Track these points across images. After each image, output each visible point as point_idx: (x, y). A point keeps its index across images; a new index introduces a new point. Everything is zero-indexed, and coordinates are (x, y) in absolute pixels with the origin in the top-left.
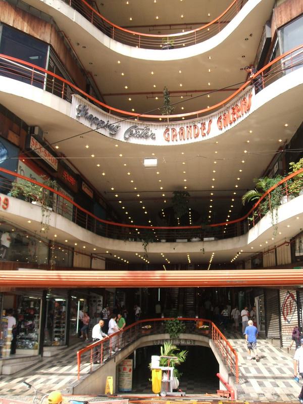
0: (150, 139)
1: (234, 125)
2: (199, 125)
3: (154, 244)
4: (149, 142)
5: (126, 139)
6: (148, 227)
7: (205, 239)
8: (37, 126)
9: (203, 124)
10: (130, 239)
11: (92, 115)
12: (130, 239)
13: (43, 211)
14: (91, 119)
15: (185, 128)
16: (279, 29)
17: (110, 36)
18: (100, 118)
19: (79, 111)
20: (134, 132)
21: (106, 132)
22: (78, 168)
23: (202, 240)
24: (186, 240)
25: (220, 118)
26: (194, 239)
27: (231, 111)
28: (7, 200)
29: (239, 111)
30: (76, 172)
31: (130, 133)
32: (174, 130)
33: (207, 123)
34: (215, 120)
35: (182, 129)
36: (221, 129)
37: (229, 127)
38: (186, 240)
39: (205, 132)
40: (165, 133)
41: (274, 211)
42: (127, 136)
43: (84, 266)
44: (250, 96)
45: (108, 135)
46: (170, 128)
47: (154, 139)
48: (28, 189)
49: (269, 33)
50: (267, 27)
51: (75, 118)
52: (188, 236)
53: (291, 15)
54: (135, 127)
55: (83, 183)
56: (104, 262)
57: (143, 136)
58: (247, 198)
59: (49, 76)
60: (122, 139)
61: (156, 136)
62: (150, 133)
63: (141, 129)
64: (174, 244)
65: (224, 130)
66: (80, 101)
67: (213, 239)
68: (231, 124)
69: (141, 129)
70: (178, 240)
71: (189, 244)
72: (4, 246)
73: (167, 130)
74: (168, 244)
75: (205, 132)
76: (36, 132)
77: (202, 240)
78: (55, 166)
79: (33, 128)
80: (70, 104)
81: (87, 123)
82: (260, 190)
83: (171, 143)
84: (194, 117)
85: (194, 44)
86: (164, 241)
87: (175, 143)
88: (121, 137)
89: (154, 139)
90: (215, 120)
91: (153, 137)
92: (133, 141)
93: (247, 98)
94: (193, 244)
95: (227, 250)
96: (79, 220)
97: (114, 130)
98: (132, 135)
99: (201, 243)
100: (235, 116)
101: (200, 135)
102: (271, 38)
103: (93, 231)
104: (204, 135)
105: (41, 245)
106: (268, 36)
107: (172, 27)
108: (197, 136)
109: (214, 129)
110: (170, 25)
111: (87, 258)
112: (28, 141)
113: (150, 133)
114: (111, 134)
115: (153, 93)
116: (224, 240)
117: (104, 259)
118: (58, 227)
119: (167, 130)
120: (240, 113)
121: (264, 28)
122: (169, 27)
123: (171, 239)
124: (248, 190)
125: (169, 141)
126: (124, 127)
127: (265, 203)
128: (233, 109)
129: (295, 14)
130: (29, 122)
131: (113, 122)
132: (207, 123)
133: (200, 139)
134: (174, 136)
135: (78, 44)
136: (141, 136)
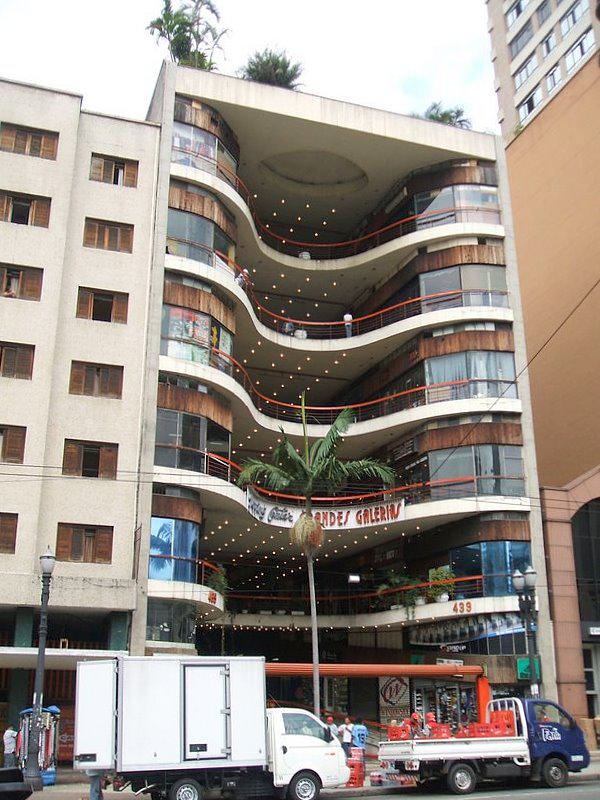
1: (375, 524)
2: (336, 515)
5: (269, 521)
24: (303, 613)
26: (280, 612)
31: (273, 516)
33: (344, 515)
37: (370, 524)
39: (342, 521)
41: (410, 609)
43: (562, 666)
47: (291, 521)
67: (303, 613)
68: (373, 521)
70: (262, 612)
71: (274, 616)
74: (253, 616)
75: (342, 521)
83: (363, 526)
84: (584, 481)
86: (246, 612)
92: (275, 523)
94: (279, 618)
95: (57, 607)
105: (44, 617)
108: (332, 524)
111: (563, 686)
123: (254, 611)
126: (269, 508)
129: (555, 580)
135: (374, 269)
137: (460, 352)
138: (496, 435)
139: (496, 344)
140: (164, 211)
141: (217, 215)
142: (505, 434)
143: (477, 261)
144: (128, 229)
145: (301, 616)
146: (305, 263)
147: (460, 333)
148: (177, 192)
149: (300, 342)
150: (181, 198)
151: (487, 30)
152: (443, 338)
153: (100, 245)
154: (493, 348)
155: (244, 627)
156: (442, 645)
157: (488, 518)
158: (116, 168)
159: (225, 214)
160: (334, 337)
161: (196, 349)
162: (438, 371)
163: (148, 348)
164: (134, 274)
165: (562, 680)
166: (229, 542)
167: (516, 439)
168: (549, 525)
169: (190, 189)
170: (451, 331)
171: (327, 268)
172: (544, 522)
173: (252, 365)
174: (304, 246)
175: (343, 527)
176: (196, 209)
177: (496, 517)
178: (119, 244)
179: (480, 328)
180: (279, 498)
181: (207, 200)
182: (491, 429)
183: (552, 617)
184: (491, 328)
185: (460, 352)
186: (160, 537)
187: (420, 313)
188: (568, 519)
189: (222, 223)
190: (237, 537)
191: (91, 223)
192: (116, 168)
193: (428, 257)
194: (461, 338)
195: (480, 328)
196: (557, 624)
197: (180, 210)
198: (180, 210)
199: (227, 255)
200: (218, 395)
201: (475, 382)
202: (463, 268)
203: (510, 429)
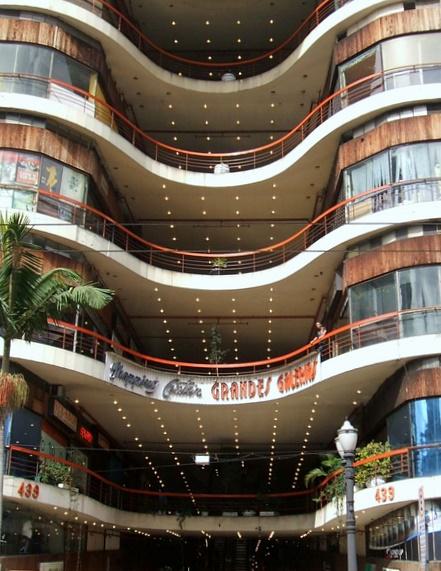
0: (195, 397)
1: (296, 390)
2: (256, 382)
3: (192, 518)
4: (194, 400)
5: (165, 396)
6: (186, 495)
7: (262, 513)
8: (60, 385)
9: (261, 381)
10: (160, 512)
11: (127, 373)
12: (160, 512)
13: (71, 495)
14: (126, 378)
15: (239, 383)
16: (349, 287)
17: (147, 261)
18: (136, 373)
19: (113, 370)
20: (175, 387)
21: (141, 391)
22: (93, 416)
23: (257, 515)
24: (236, 514)
25: (281, 378)
26: (247, 513)
27: (294, 373)
28: (37, 487)
29: (302, 376)
30: (91, 422)
31: (169, 387)
32: (224, 385)
33: (266, 380)
34: (275, 379)
35: (234, 384)
36: (282, 392)
37: (291, 392)
38: (236, 514)
39: (263, 391)
40: (213, 388)
42: (166, 394)
44: (315, 363)
45: (144, 395)
46: (220, 382)
47: (200, 396)
48: (56, 468)
49: (341, 284)
50: (338, 277)
51: (108, 380)
52: (239, 509)
53: (362, 274)
54: (177, 380)
55: (100, 435)
56: (119, 539)
57: (186, 393)
58: (310, 479)
59: (79, 333)
60: (162, 398)
61: (203, 393)
62: (194, 389)
63: (184, 383)
64: (219, 519)
65: (285, 394)
66: (114, 358)
67: (272, 513)
68: (293, 388)
69: (184, 383)
70: (225, 514)
71: (240, 519)
72: (26, 537)
73: (217, 384)
74: (211, 520)
75: (263, 391)
76: (60, 393)
77: (257, 515)
78: (73, 426)
79: (56, 387)
80: (99, 363)
81: (120, 384)
82: (326, 469)
83: (220, 402)
85: (251, 270)
86: (205, 514)
87: (225, 402)
88: (159, 395)
89: (200, 396)
90: (275, 379)
91: (199, 393)
92: (175, 399)
93: (312, 364)
96: (95, 491)
97: (150, 386)
98: (172, 391)
99: (256, 518)
100: (298, 381)
101: (257, 395)
102: (341, 291)
103: (107, 504)
104: (261, 396)
106: (339, 288)
107: (225, 135)
108: (252, 395)
109: (273, 389)
110: (222, 132)
112: (51, 408)
113: (194, 389)
114: (148, 393)
115: (233, 132)
116: (287, 517)
117: (118, 534)
118: (86, 512)
119: (217, 384)
120: (303, 379)
121: (334, 276)
122: (219, 223)
123: (215, 512)
124: (313, 468)
125: (217, 399)
126: (163, 381)
127: (332, 487)
128: (296, 371)
130: (50, 381)
131: (151, 377)
132: (266, 380)
133: (256, 399)
134: (226, 393)
135: (108, 274)
136: (183, 393)
139: (427, 132)
141: (57, 39)
143: (401, 32)
145: (234, 517)
146: (229, 85)
149: (221, 178)
150: (10, 27)
154: (423, 137)
155: (132, 530)
156: (388, 548)
160: (259, 165)
161: (18, 195)
166: (307, 437)
171: (259, 85)
174: (224, 67)
175: (265, 399)
176: (28, 36)
180: (221, 370)
181: (44, 27)
182: (420, 245)
187: (341, 109)
190: (309, 430)
194: (383, 134)
198: (7, 42)
199: (88, 91)
201: (399, 188)
202: (383, 44)
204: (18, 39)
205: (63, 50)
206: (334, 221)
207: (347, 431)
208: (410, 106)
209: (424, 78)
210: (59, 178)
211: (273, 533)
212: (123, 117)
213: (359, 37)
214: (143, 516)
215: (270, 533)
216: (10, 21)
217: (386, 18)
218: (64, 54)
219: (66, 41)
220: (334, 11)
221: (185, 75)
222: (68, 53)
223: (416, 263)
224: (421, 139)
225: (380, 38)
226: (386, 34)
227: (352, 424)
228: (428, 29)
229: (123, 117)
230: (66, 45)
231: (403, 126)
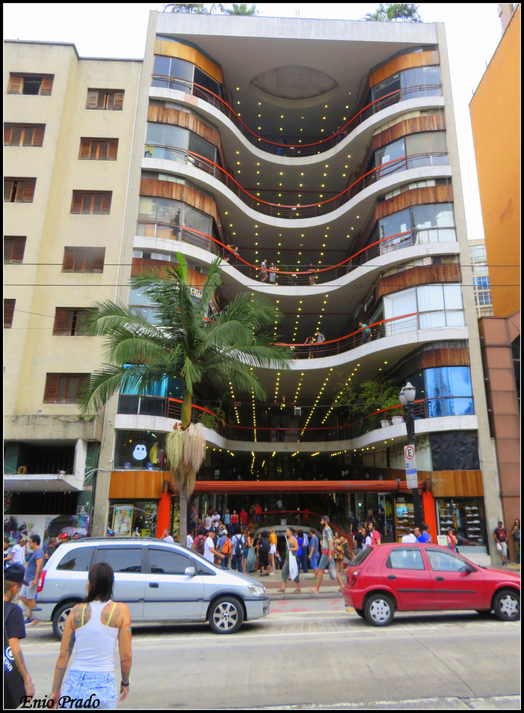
111: (504, 499)
115: (295, 192)
137: (405, 208)
138: (435, 275)
140: (145, 126)
141: (191, 123)
142: (444, 273)
143: (419, 130)
144: (113, 143)
147: (404, 193)
148: (156, 109)
151: (497, 15)
152: (392, 200)
153: (93, 158)
154: (432, 200)
157: (430, 348)
158: (107, 98)
159: (202, 123)
162: (394, 306)
163: (122, 233)
164: (117, 176)
165: (505, 493)
167: (454, 276)
168: (489, 351)
169: (167, 106)
170: (397, 193)
172: (483, 348)
173: (225, 236)
177: (441, 346)
178: (108, 155)
179: (422, 185)
183: (493, 434)
184: (432, 184)
185: (405, 208)
186: (271, 368)
188: (509, 343)
189: (200, 130)
191: (85, 142)
192: (107, 98)
193: (386, 136)
195: (422, 185)
196: (498, 441)
197: (158, 122)
198: (158, 122)
200: (197, 268)
203: (449, 269)
204: (164, 121)
205: (195, 131)
206: (375, 253)
207: (410, 389)
208: (425, 180)
209: (91, 156)
210: (200, 131)
211: (274, 453)
212: (232, 178)
213: (390, 131)
214: (242, 443)
215: (272, 453)
216: (159, 109)
217: (409, 120)
218: (196, 134)
219: (197, 125)
220: (372, 114)
221: (322, 152)
222: (198, 133)
223: (428, 281)
224: (431, 202)
225: (405, 134)
226: (409, 132)
227: (412, 384)
228: (436, 129)
229: (232, 178)
230: (197, 128)
231: (420, 193)
